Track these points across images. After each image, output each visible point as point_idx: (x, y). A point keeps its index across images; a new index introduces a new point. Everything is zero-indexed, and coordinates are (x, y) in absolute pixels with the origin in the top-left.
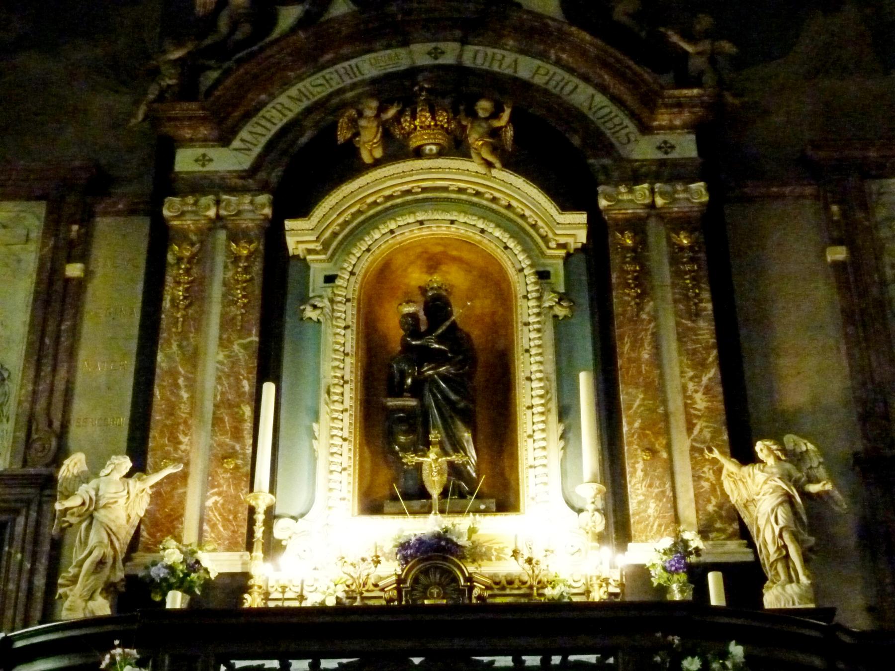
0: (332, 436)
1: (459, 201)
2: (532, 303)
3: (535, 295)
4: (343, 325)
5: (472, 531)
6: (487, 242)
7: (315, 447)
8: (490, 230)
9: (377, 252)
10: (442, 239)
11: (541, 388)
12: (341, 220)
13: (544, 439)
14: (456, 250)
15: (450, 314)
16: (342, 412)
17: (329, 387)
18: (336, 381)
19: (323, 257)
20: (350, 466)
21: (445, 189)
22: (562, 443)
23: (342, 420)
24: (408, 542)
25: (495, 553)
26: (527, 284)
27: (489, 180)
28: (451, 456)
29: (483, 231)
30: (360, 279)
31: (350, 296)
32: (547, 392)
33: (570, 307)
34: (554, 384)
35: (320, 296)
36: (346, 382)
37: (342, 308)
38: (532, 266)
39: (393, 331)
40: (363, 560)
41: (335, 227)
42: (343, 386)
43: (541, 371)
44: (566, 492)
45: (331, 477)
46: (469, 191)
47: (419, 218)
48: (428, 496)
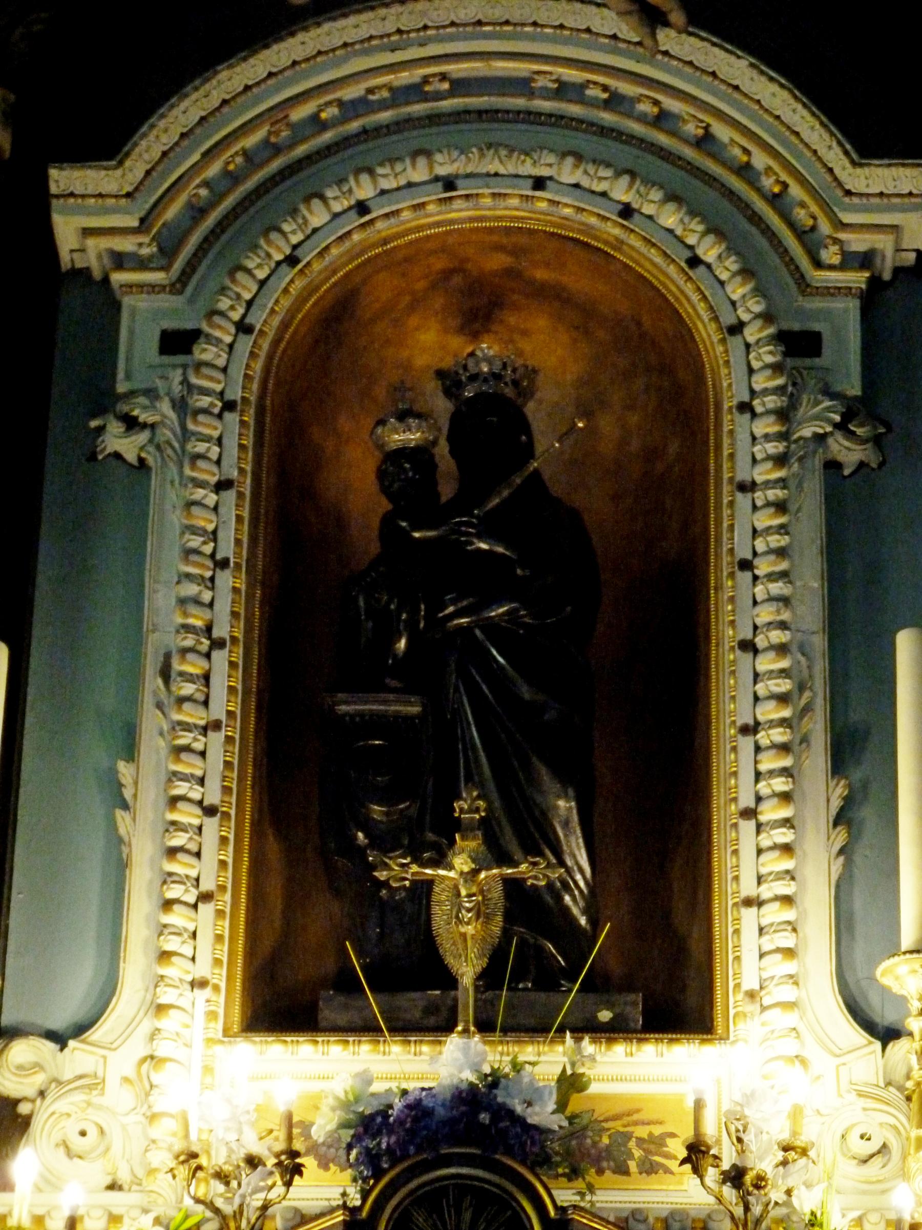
0: (174, 801)
1: (557, 120)
2: (765, 426)
3: (772, 401)
4: (214, 480)
5: (571, 1084)
6: (638, 244)
7: (122, 831)
8: (648, 209)
9: (317, 266)
10: (508, 231)
11: (784, 673)
12: (213, 170)
13: (787, 823)
14: (547, 265)
15: (528, 452)
16: (205, 730)
17: (168, 656)
18: (189, 642)
19: (157, 277)
20: (222, 888)
21: (523, 86)
22: (840, 837)
23: (203, 754)
24: (384, 1113)
25: (637, 1153)
26: (751, 371)
27: (651, 62)
28: (516, 864)
29: (627, 211)
30: (265, 345)
31: (234, 393)
32: (801, 687)
33: (877, 441)
34: (821, 667)
35: (151, 394)
36: (219, 644)
37: (207, 427)
38: (767, 317)
39: (355, 483)
40: (253, 1162)
41: (196, 191)
42: (208, 656)
43: (783, 626)
44: (851, 980)
45: (166, 919)
46: (592, 92)
47: (442, 171)
48: (450, 981)
